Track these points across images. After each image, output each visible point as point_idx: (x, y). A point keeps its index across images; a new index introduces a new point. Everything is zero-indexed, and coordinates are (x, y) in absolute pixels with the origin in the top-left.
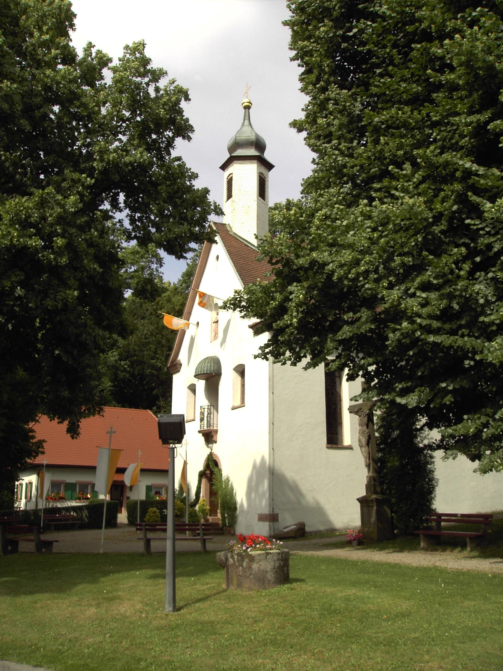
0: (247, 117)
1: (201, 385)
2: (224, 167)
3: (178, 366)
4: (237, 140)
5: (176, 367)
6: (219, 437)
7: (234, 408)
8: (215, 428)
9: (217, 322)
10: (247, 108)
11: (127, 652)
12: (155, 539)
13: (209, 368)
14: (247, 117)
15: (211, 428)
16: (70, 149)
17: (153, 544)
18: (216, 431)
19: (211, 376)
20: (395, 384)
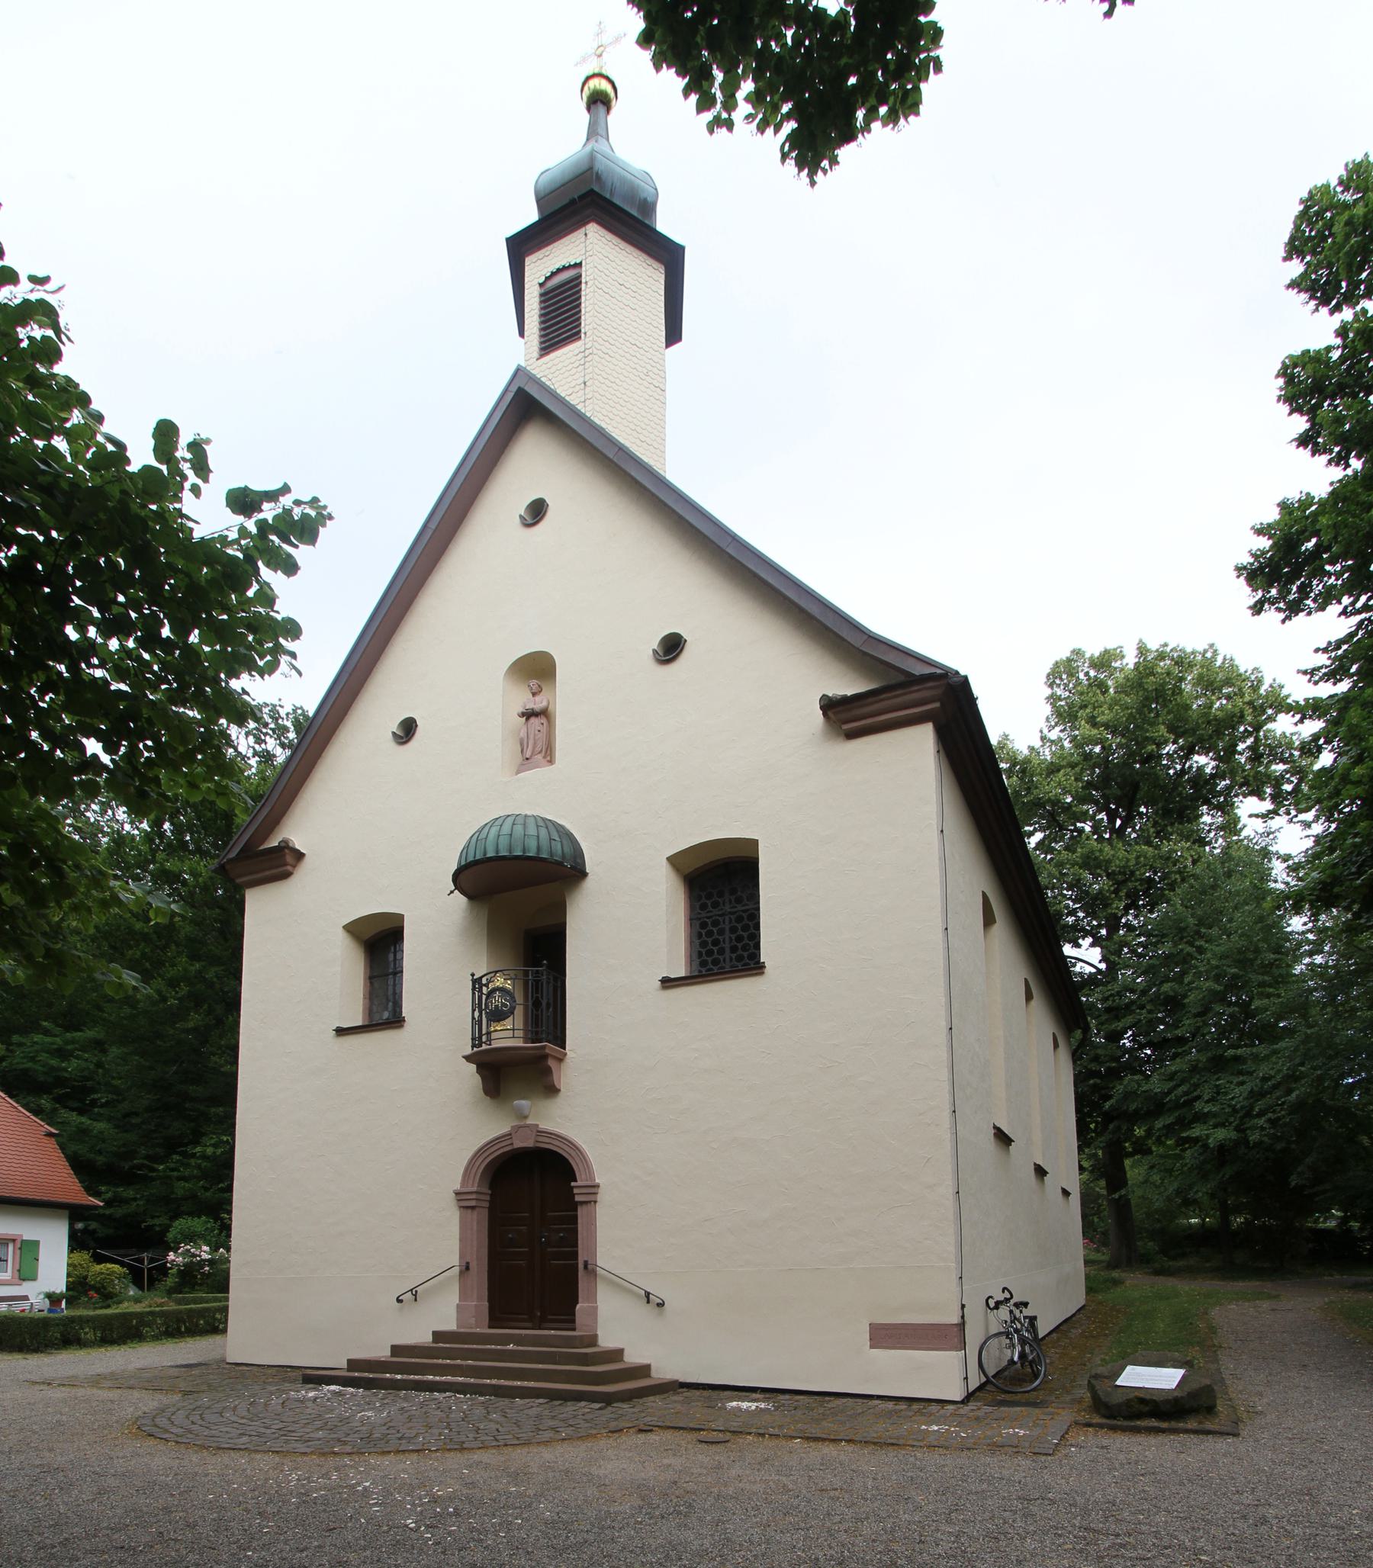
14: (596, 131)
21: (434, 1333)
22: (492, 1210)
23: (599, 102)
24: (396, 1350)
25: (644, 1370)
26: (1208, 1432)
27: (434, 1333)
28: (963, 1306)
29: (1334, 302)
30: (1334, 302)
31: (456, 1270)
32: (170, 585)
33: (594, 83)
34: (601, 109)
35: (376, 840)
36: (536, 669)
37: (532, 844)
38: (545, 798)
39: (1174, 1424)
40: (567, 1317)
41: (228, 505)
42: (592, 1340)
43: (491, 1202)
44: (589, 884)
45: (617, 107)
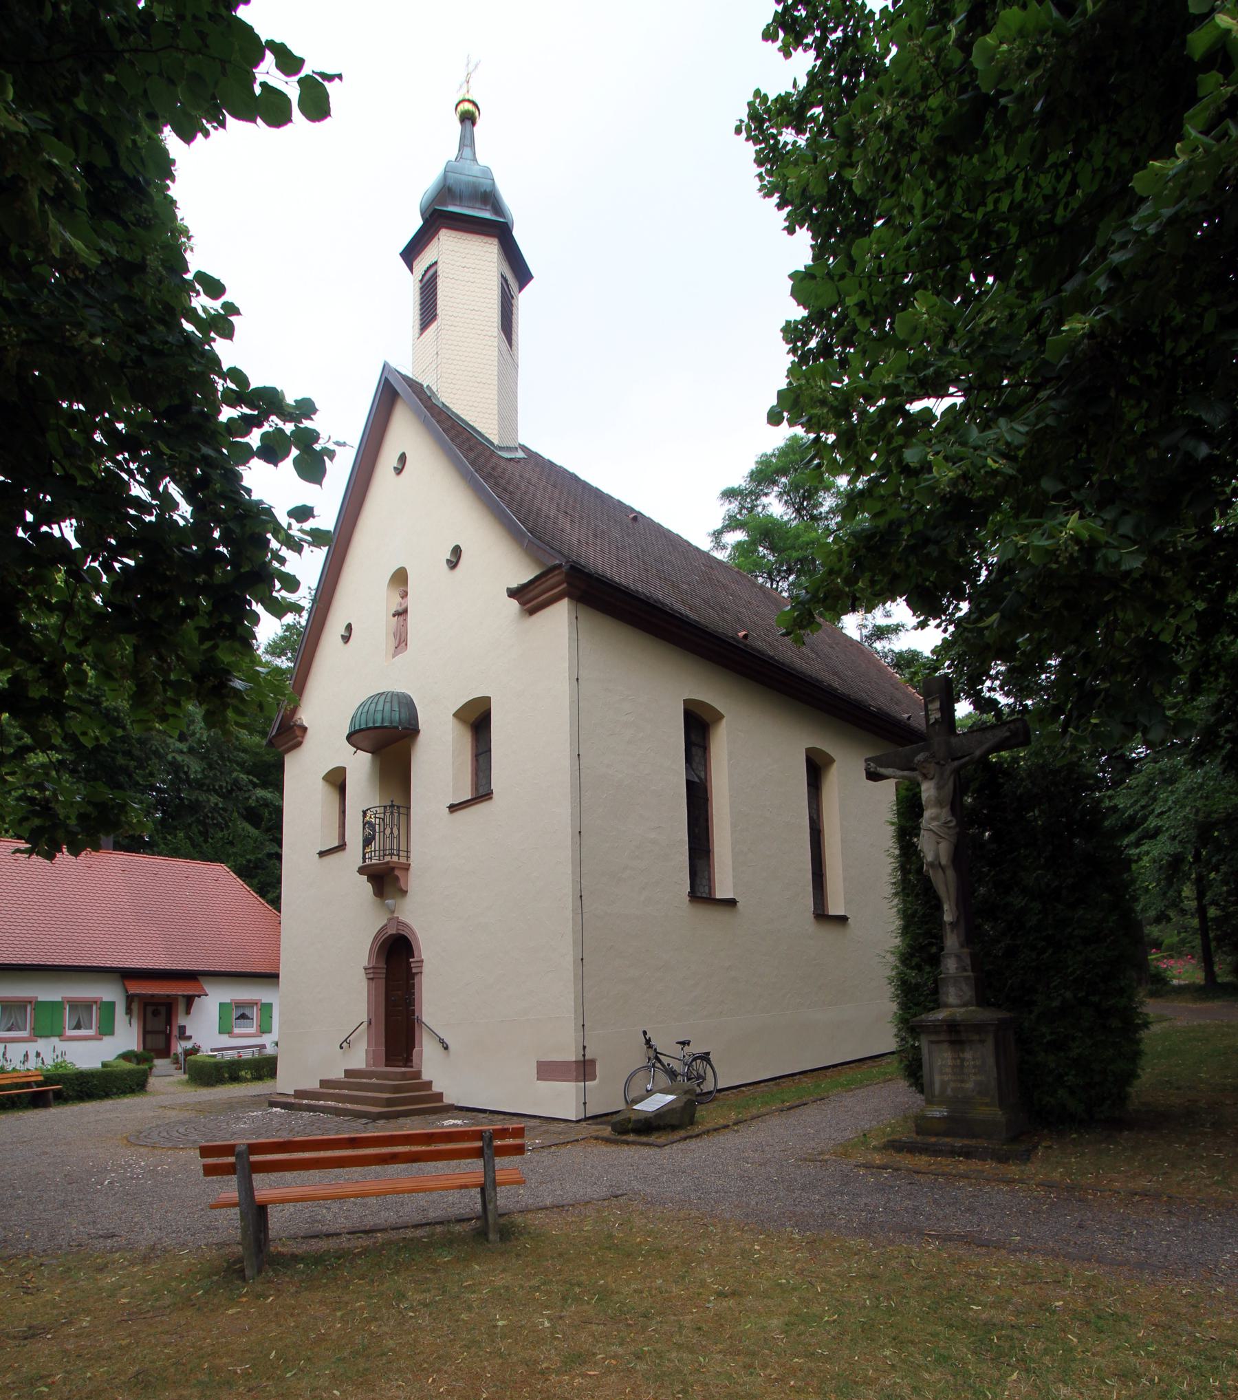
0: (467, 142)
1: (359, 765)
2: (410, 254)
3: (298, 732)
4: (450, 182)
5: (291, 734)
6: (415, 882)
7: (453, 808)
8: (403, 860)
9: (405, 611)
10: (468, 119)
11: (45, 291)
12: (284, 1201)
13: (387, 714)
14: (467, 142)
15: (395, 859)
16: (30, 517)
17: (276, 1218)
18: (406, 868)
19: (388, 738)
20: (943, 650)
21: (346, 1071)
22: (387, 979)
23: (468, 119)
24: (324, 1083)
25: (439, 1096)
26: (691, 1137)
27: (346, 1071)
28: (584, 1047)
29: (125, 477)
30: (125, 477)
31: (365, 1024)
32: (1202, 229)
33: (461, 108)
34: (468, 123)
35: (328, 710)
36: (400, 578)
37: (379, 717)
38: (397, 677)
39: (644, 1139)
40: (408, 1061)
41: (792, 294)
42: (418, 1075)
43: (387, 973)
44: (422, 738)
45: (479, 122)
